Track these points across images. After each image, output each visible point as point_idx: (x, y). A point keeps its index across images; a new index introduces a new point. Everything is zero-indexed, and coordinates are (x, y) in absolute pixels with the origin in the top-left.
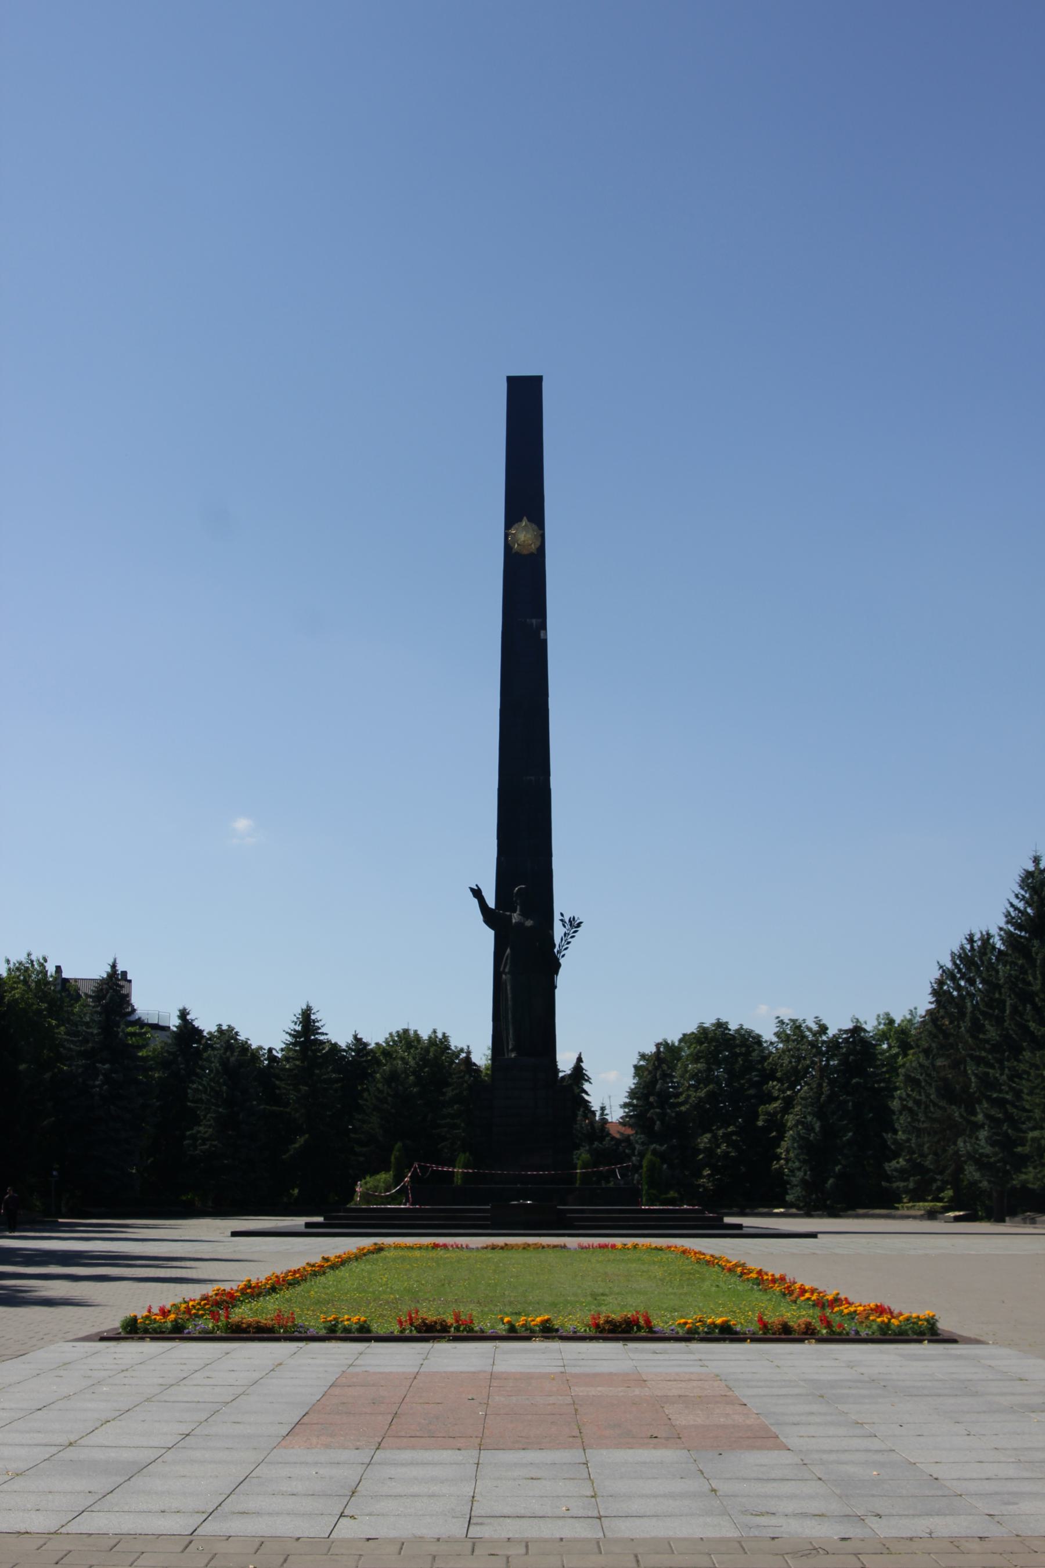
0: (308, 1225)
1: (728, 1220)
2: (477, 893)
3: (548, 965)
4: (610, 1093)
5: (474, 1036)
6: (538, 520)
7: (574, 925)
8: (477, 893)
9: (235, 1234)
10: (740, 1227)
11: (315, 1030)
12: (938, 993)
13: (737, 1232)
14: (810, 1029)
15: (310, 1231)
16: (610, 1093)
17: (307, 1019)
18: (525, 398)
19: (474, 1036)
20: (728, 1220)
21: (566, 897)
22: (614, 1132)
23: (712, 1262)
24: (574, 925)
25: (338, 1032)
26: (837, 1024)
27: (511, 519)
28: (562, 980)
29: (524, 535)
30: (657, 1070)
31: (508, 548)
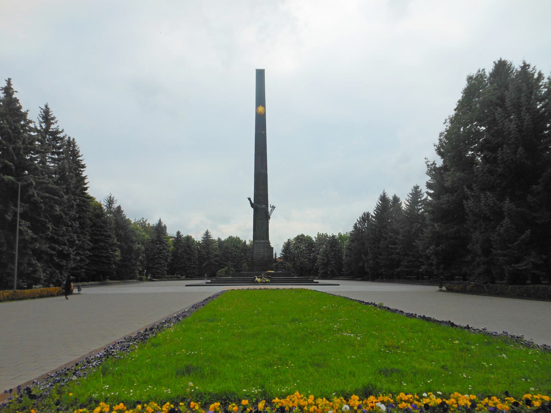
0: (206, 283)
1: (315, 281)
2: (249, 199)
3: (267, 217)
4: (278, 250)
5: (247, 237)
6: (264, 105)
7: (273, 207)
8: (249, 199)
9: (187, 286)
10: (318, 282)
11: (209, 236)
12: (355, 227)
13: (317, 284)
14: (372, 216)
15: (207, 284)
16: (278, 250)
17: (207, 233)
18: (260, 74)
19: (247, 237)
20: (315, 281)
21: (271, 201)
22: (278, 260)
23: (332, 296)
24: (273, 207)
25: (215, 236)
26: (330, 234)
27: (257, 105)
28: (271, 222)
29: (261, 109)
30: (287, 246)
31: (256, 113)
